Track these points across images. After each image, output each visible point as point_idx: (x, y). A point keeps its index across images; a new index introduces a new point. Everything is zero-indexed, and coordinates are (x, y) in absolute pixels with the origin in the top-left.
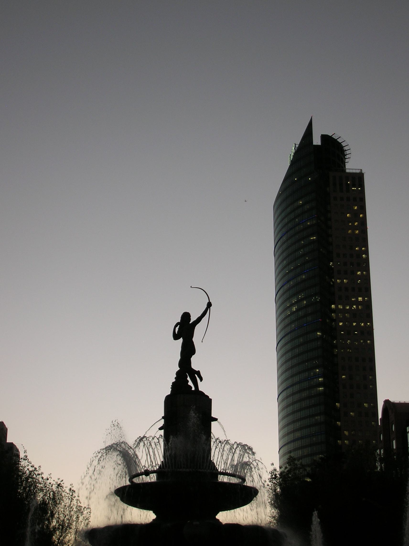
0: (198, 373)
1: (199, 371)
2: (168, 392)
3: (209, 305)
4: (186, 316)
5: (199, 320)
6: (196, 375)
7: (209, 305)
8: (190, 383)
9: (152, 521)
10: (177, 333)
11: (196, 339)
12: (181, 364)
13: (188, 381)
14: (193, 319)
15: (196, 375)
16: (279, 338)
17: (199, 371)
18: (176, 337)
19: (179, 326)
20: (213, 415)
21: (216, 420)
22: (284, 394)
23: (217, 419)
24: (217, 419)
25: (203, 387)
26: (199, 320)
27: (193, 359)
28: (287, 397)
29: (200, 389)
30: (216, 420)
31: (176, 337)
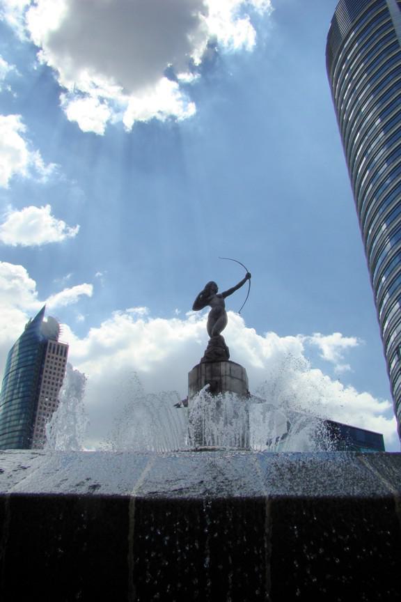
3: (248, 276)
4: (211, 288)
7: (248, 276)
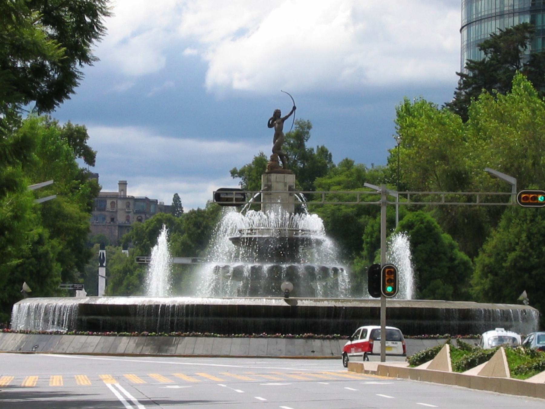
3: (294, 108)
4: (277, 114)
5: (287, 117)
7: (294, 108)
14: (282, 116)
26: (287, 117)
31: (270, 126)
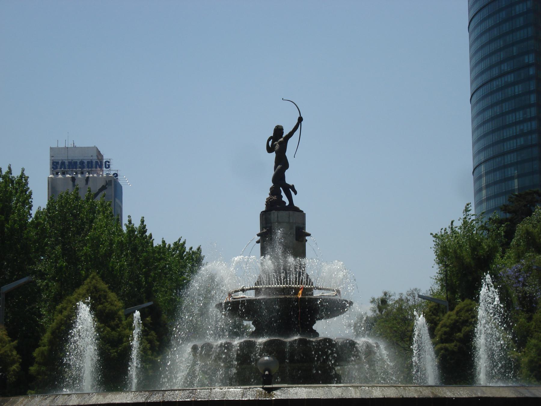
0: (293, 187)
1: (293, 185)
2: (263, 208)
3: (300, 120)
4: (278, 131)
5: (291, 134)
6: (290, 189)
7: (300, 120)
8: (285, 198)
9: (98, 191)
10: (270, 146)
11: (289, 154)
12: (275, 180)
13: (282, 197)
14: (286, 133)
15: (290, 189)
16: (473, 12)
17: (293, 185)
18: (270, 150)
19: (272, 140)
20: (307, 230)
21: (309, 235)
22: (480, 93)
23: (310, 234)
24: (310, 234)
25: (297, 202)
26: (291, 134)
27: (287, 173)
28: (484, 97)
29: (296, 204)
30: (309, 235)
31: (270, 150)
